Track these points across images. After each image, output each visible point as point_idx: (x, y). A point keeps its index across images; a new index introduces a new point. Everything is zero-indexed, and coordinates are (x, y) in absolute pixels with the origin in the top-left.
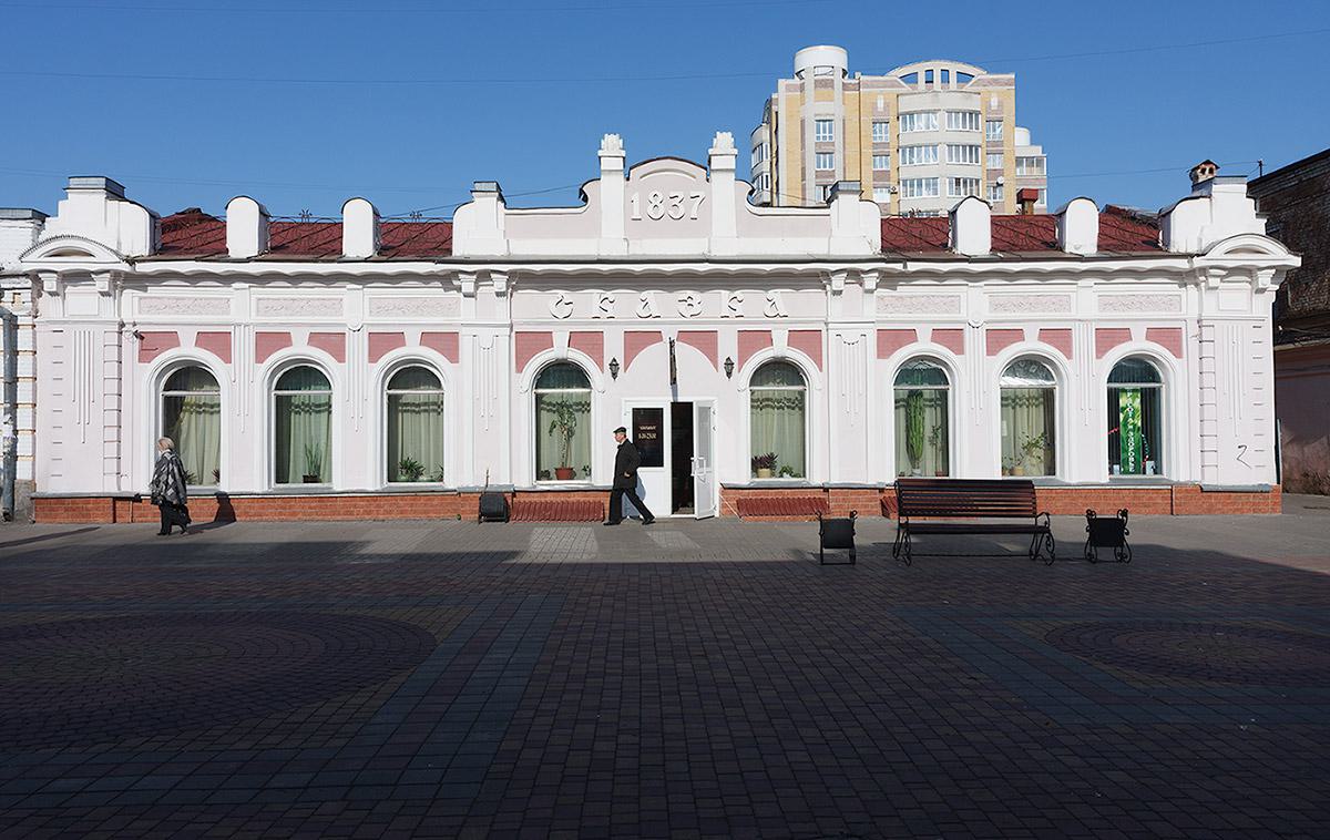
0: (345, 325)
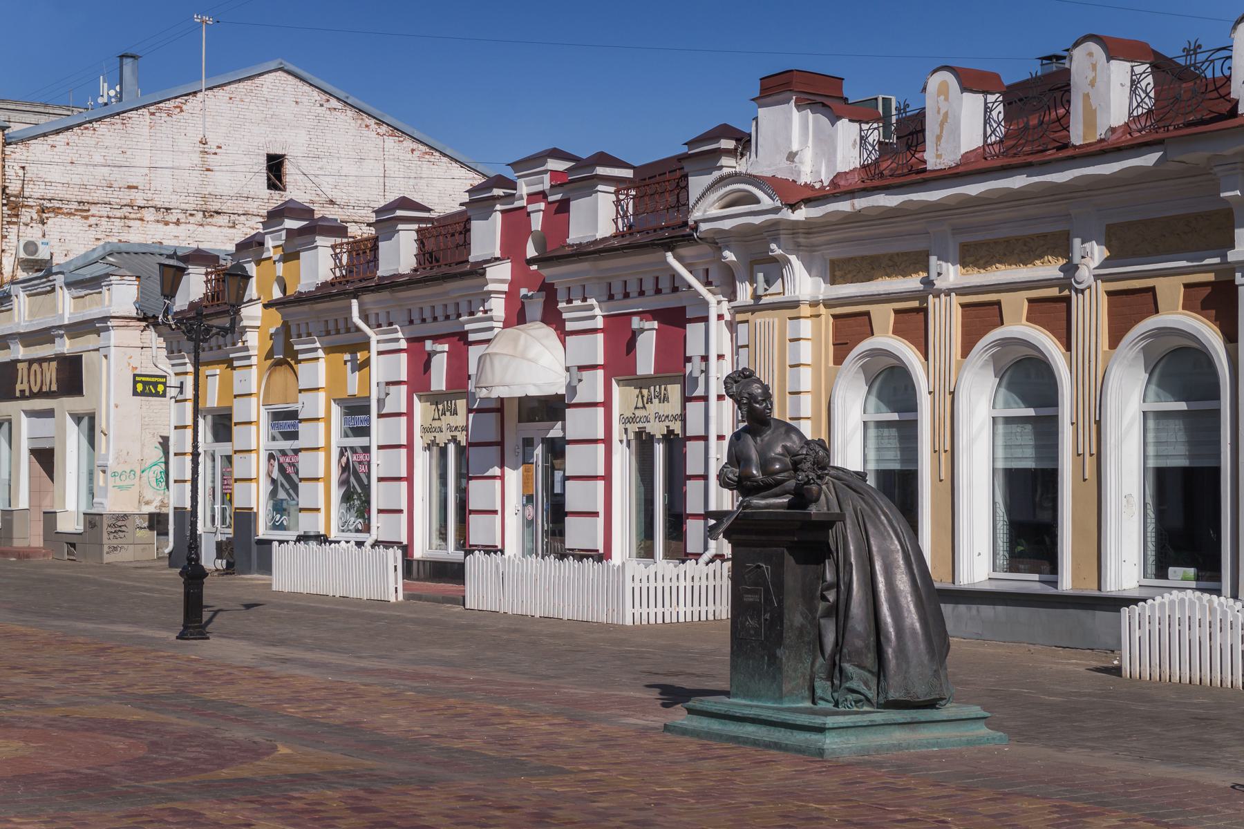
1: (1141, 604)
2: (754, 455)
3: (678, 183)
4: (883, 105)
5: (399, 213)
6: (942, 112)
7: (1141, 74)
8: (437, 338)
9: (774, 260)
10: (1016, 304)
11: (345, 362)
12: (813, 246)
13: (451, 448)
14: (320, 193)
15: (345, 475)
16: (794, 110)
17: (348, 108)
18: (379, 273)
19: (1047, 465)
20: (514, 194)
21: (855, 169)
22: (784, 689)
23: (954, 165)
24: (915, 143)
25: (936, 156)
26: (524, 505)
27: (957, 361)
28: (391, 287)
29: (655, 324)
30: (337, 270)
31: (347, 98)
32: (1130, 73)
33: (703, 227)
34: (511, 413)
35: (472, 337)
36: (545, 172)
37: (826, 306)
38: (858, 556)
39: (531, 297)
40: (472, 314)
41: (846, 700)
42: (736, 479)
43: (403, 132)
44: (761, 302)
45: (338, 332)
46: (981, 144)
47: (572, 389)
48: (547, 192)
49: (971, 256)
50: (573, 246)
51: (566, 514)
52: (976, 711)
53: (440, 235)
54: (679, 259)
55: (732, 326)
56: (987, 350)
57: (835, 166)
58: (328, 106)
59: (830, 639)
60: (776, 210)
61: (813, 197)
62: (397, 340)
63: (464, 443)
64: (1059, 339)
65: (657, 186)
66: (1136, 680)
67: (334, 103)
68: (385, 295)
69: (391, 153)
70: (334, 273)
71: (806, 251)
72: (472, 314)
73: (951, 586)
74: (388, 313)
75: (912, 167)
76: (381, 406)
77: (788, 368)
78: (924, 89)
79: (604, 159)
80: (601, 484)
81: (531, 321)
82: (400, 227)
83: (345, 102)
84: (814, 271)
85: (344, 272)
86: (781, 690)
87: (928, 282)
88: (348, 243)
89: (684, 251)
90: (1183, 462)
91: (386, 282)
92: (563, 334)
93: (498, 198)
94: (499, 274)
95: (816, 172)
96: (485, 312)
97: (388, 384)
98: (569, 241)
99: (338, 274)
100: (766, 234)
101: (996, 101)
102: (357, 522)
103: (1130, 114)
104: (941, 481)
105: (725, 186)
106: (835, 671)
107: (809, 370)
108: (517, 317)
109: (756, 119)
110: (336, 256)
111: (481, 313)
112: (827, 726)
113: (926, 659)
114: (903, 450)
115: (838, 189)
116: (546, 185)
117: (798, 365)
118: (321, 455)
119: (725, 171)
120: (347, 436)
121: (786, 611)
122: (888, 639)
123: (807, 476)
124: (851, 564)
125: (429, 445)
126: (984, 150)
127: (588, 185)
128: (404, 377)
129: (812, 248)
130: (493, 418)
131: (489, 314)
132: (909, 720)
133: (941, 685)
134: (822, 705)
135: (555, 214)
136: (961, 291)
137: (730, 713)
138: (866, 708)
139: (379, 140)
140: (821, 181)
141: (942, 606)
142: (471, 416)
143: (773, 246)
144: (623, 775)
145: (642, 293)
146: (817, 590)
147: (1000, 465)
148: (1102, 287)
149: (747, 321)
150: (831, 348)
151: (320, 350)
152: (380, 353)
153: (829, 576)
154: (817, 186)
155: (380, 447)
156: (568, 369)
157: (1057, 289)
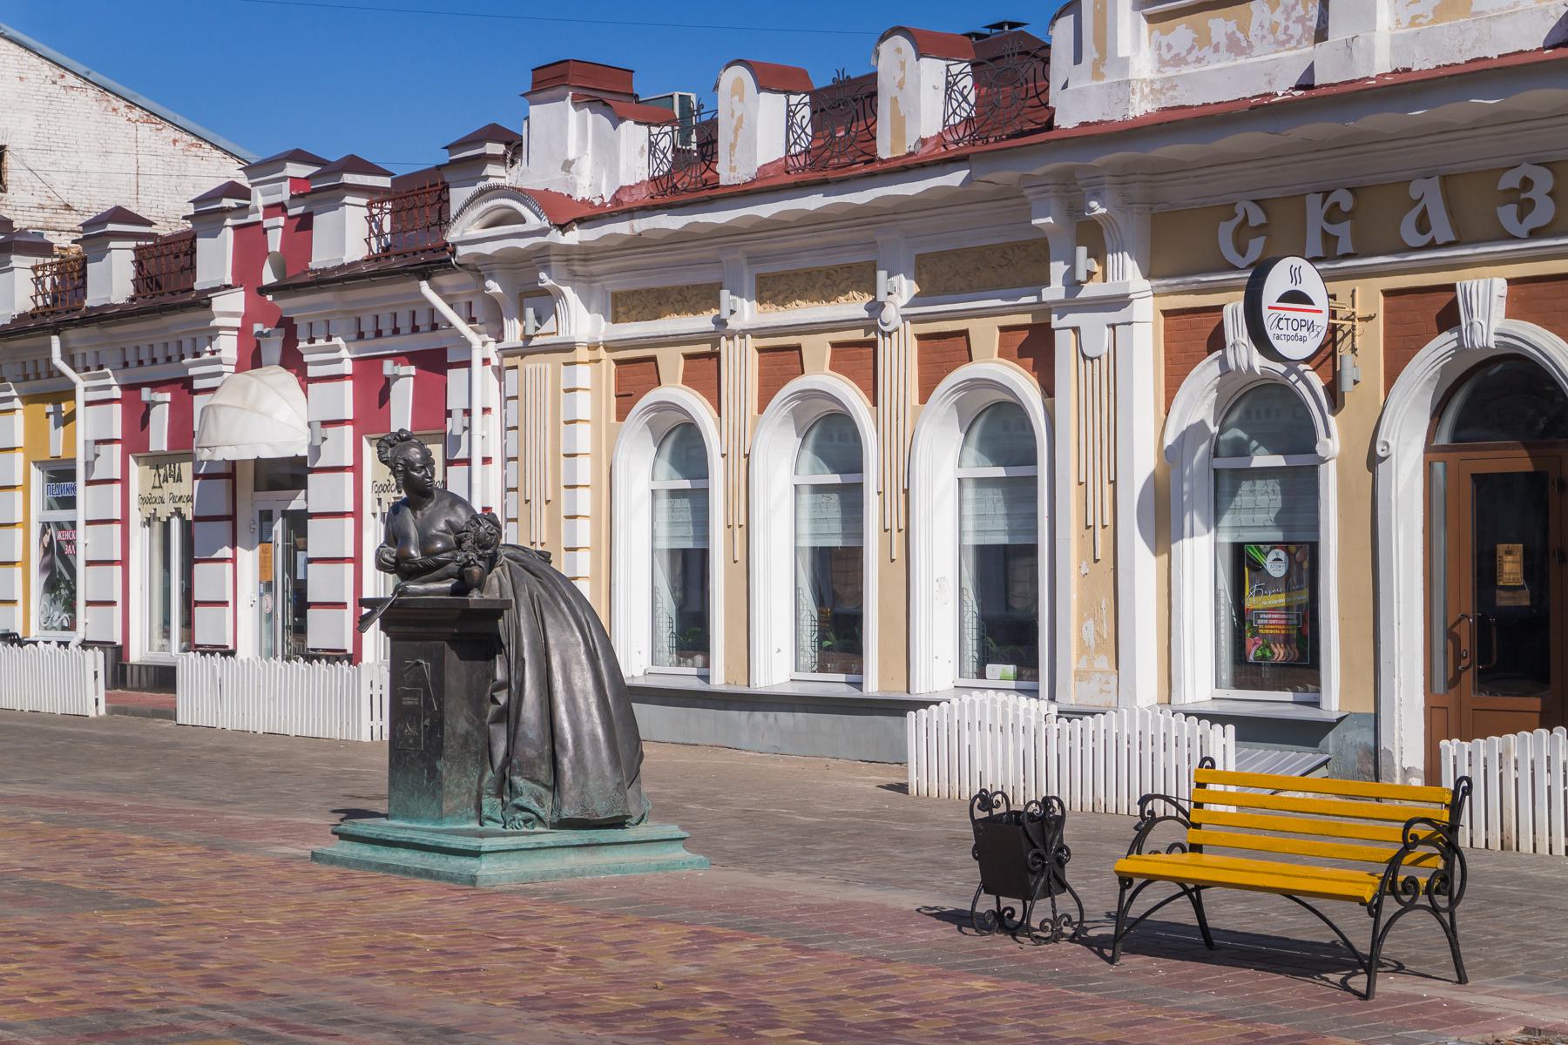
1: (933, 707)
2: (413, 533)
3: (440, 195)
4: (681, 104)
5: (111, 227)
6: (737, 115)
7: (957, 75)
8: (156, 385)
9: (545, 292)
10: (817, 349)
11: (48, 415)
12: (592, 276)
13: (175, 524)
14: (53, 195)
15: (48, 558)
16: (571, 108)
17: (89, 86)
18: (88, 303)
19: (852, 543)
20: (247, 206)
21: (642, 183)
22: (444, 807)
23: (749, 180)
24: (709, 153)
25: (732, 169)
26: (261, 595)
27: (754, 418)
28: (98, 321)
29: (412, 370)
30: (39, 297)
31: (88, 73)
32: (945, 74)
33: (462, 251)
34: (246, 479)
35: (198, 384)
36: (284, 179)
37: (607, 349)
38: (534, 649)
39: (268, 335)
40: (197, 355)
41: (514, 819)
42: (393, 560)
43: (162, 118)
44: (1082, 295)
45: (38, 377)
46: (782, 155)
47: (316, 451)
48: (287, 204)
49: (771, 289)
50: (316, 271)
51: (310, 605)
52: (673, 830)
53: (162, 255)
54: (437, 289)
55: (500, 372)
56: (785, 405)
57: (618, 179)
58: (61, 82)
59: (500, 749)
60: (543, 232)
61: (590, 216)
62: (109, 387)
63: (189, 517)
64: (865, 391)
65: (415, 198)
66: (934, 799)
67: (70, 79)
68: (92, 330)
69: (145, 144)
70: (35, 302)
71: (585, 282)
72: (197, 355)
73: (745, 690)
74: (97, 353)
75: (706, 180)
76: (90, 471)
77: (562, 425)
78: (716, 87)
79: (356, 164)
80: (349, 568)
81: (268, 365)
82: (112, 244)
83: (85, 79)
84: (593, 306)
85: (48, 301)
86: (440, 808)
87: (720, 322)
88: (52, 265)
89: (443, 280)
90: (1002, 539)
91: (94, 314)
92: (305, 381)
93: (229, 210)
94: (230, 306)
95: (596, 186)
96: (213, 353)
97: (98, 442)
98: (313, 265)
99: (40, 303)
100: (534, 261)
101: (799, 104)
102: (62, 617)
103: (944, 122)
104: (892, 560)
105: (487, 200)
106: (504, 786)
107: (588, 427)
108: (252, 359)
109: (527, 118)
110: (38, 281)
111: (208, 355)
112: (482, 849)
113: (608, 769)
114: (844, 522)
115: (620, 209)
116: (284, 194)
117: (574, 422)
118: (18, 533)
119: (491, 181)
120: (51, 508)
121: (447, 716)
122: (564, 748)
123: (466, 557)
124: (523, 660)
125: (148, 519)
126: (786, 161)
127: (331, 196)
128: (118, 435)
129: (590, 278)
130: (222, 485)
131: (218, 355)
132: (586, 842)
133: (625, 800)
134: (490, 825)
135: (297, 231)
136: (757, 333)
137: (383, 837)
138: (537, 829)
139: (131, 128)
140: (602, 197)
141: (634, 705)
142: (197, 482)
143: (543, 275)
144: (219, 908)
145: (396, 331)
146: (486, 691)
147: (970, 540)
148: (912, 330)
149: (516, 367)
150: (614, 400)
151: (17, 400)
152: (88, 404)
153: (500, 674)
154: (597, 202)
155: (89, 523)
156: (309, 425)
157: (862, 331)
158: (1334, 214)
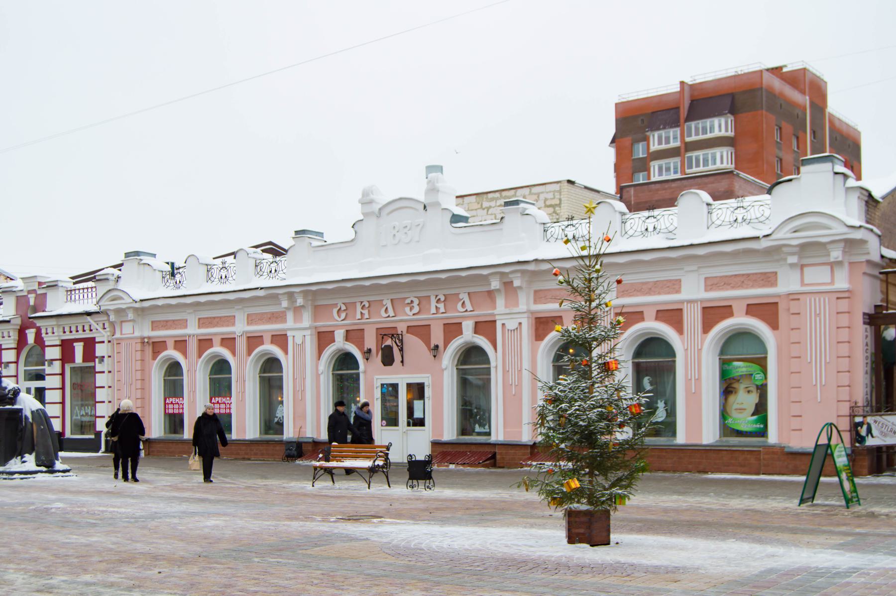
0: (235, 333)
158: (363, 307)
